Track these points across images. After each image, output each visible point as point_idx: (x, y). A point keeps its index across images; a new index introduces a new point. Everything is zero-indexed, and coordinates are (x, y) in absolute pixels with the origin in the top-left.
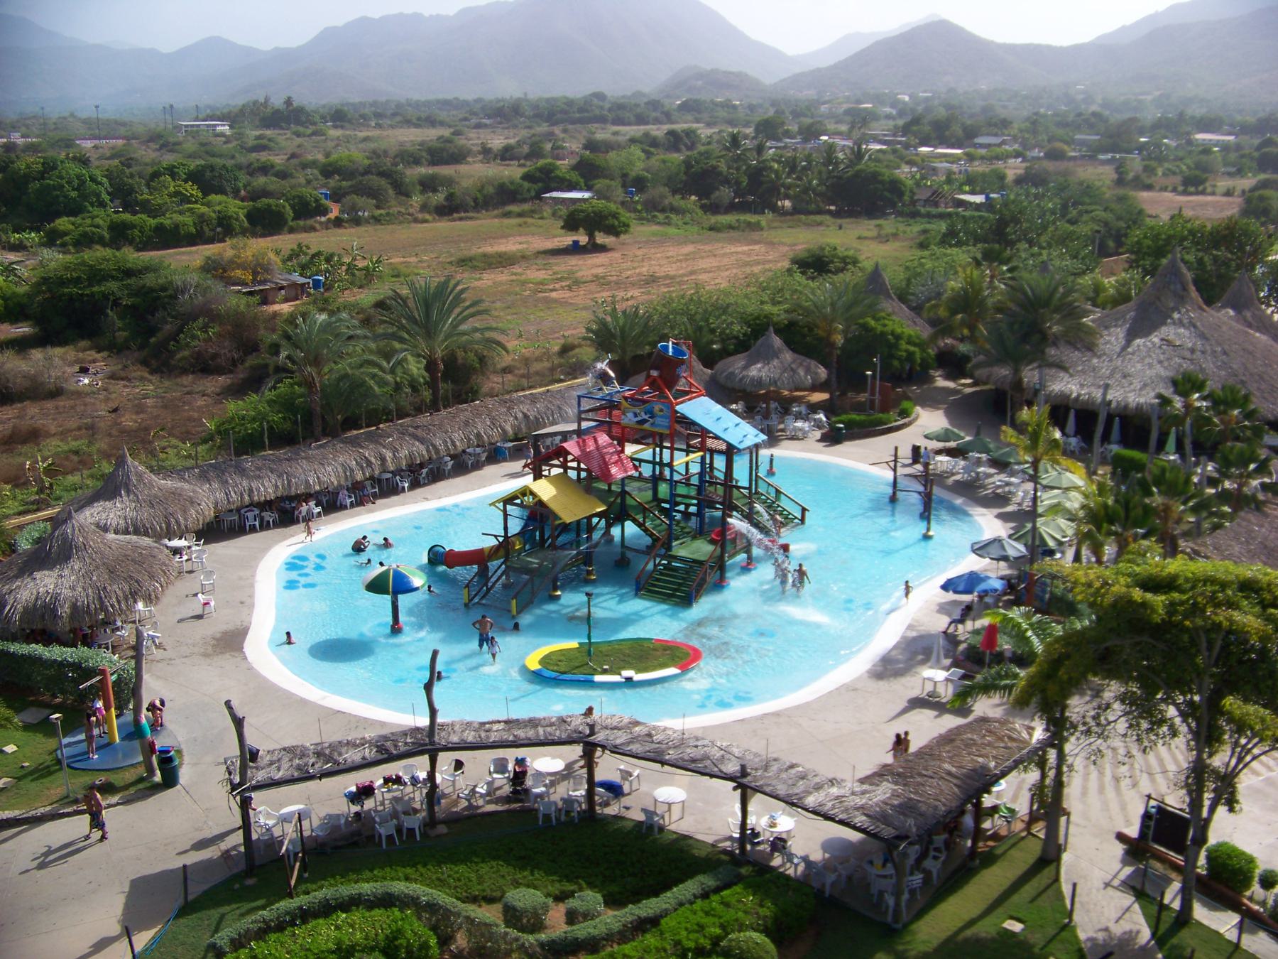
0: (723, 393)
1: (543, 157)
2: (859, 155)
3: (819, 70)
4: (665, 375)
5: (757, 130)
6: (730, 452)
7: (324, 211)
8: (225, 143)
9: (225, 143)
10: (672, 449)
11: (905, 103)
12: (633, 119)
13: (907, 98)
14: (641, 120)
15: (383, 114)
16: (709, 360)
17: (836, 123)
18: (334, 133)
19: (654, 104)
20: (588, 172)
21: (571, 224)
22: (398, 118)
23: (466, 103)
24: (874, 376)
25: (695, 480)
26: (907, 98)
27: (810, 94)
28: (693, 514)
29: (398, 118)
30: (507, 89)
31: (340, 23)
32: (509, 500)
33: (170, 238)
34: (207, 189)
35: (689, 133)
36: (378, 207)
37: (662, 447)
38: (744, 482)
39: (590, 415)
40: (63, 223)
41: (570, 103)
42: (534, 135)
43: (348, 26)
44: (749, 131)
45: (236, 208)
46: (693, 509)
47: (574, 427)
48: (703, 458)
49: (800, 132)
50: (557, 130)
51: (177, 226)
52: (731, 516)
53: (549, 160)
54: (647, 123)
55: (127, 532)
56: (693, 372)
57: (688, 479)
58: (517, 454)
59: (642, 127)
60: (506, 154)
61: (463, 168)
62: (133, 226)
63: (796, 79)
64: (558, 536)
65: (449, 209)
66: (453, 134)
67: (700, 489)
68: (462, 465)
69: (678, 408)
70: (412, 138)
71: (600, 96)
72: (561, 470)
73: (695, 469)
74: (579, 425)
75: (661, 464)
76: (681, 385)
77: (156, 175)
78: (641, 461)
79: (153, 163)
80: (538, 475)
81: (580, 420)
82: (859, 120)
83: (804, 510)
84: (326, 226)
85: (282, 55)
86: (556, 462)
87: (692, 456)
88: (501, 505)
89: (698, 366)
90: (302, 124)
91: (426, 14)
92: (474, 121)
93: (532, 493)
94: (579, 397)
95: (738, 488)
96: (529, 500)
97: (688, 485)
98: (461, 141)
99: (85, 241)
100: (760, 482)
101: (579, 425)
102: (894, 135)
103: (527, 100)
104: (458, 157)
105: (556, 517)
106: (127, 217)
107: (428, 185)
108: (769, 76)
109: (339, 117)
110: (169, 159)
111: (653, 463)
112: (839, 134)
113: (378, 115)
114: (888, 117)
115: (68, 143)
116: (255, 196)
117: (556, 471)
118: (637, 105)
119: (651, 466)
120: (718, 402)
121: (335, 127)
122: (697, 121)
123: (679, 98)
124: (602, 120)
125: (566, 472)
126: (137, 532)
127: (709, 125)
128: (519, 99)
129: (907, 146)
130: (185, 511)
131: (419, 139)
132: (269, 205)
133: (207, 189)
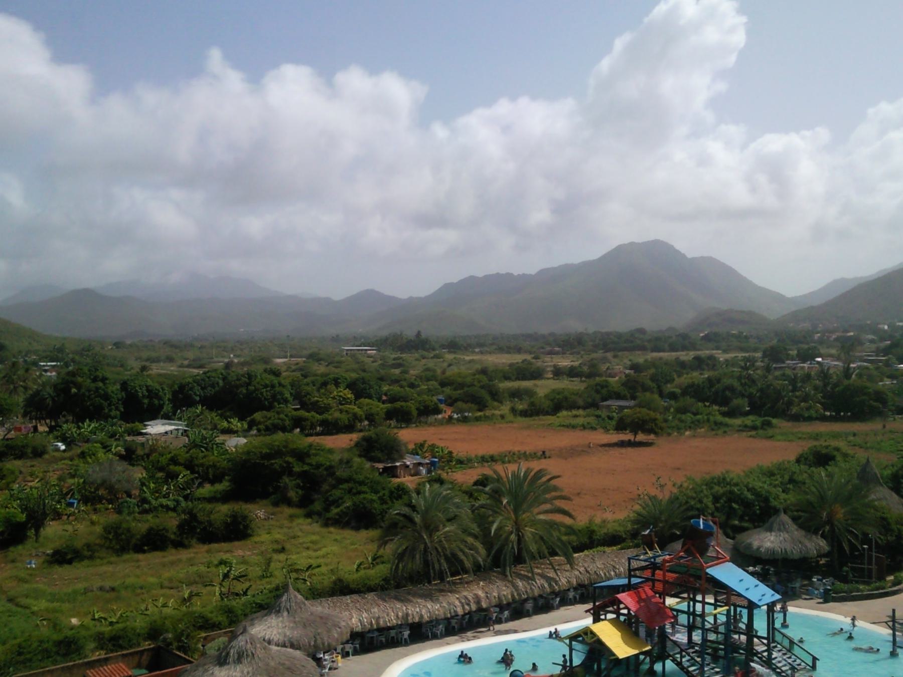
0: (744, 558)
1: (600, 375)
2: (847, 373)
3: (812, 308)
4: (697, 542)
5: (765, 355)
6: (751, 606)
7: (438, 411)
8: (373, 362)
9: (373, 362)
10: (704, 603)
11: (885, 331)
12: (666, 346)
13: (886, 327)
14: (673, 349)
15: (480, 344)
16: (732, 531)
17: (828, 348)
18: (450, 357)
19: (684, 336)
20: (632, 388)
21: (621, 427)
22: (495, 347)
23: (543, 336)
24: (870, 549)
25: (722, 629)
26: (886, 327)
27: (807, 325)
28: (721, 657)
29: (495, 347)
30: (574, 326)
31: (455, 280)
32: (574, 637)
33: (332, 428)
34: (359, 394)
35: (711, 357)
36: (480, 410)
37: (695, 601)
38: (763, 632)
39: (638, 573)
40: (258, 416)
41: (619, 336)
42: (592, 360)
43: (461, 282)
44: (759, 355)
45: (380, 408)
46: (722, 653)
47: (624, 581)
48: (729, 611)
49: (798, 355)
50: (609, 355)
51: (337, 420)
52: (753, 661)
53: (604, 378)
54: (677, 351)
55: (284, 646)
56: (719, 544)
57: (717, 628)
58: (583, 600)
59: (674, 354)
60: (572, 373)
61: (539, 382)
62: (306, 419)
63: (795, 316)
64: (611, 669)
65: (533, 411)
66: (533, 358)
67: (727, 635)
68: (544, 605)
69: (708, 571)
70: (504, 361)
71: (642, 331)
72: (614, 616)
73: (722, 619)
74: (629, 581)
75: (694, 614)
76: (711, 553)
77: (324, 384)
78: (678, 611)
79: (323, 375)
80: (596, 620)
81: (630, 577)
82: (848, 346)
83: (815, 659)
84: (441, 423)
85: (412, 304)
86: (611, 609)
87: (719, 610)
88: (567, 641)
89: (722, 538)
90: (427, 350)
91: (516, 274)
92: (548, 349)
93: (592, 633)
94: (629, 559)
95: (759, 638)
96: (588, 639)
97: (716, 632)
98: (539, 363)
99: (272, 429)
100: (776, 633)
101: (629, 581)
102: (877, 356)
103: (587, 334)
104: (537, 375)
105: (612, 653)
106: (303, 413)
107: (515, 394)
108: (774, 313)
109: (453, 346)
110: (334, 372)
111: (688, 613)
112: (831, 356)
113: (480, 345)
114: (872, 341)
115: (266, 361)
116: (393, 399)
117: (611, 616)
118: (670, 337)
119: (686, 616)
120: (739, 566)
121: (450, 352)
122: (717, 348)
123: (702, 331)
124: (643, 348)
125: (618, 617)
126: (292, 646)
127: (725, 351)
128: (581, 333)
129: (887, 364)
130: (329, 631)
131: (509, 362)
132: (402, 406)
133: (359, 394)
